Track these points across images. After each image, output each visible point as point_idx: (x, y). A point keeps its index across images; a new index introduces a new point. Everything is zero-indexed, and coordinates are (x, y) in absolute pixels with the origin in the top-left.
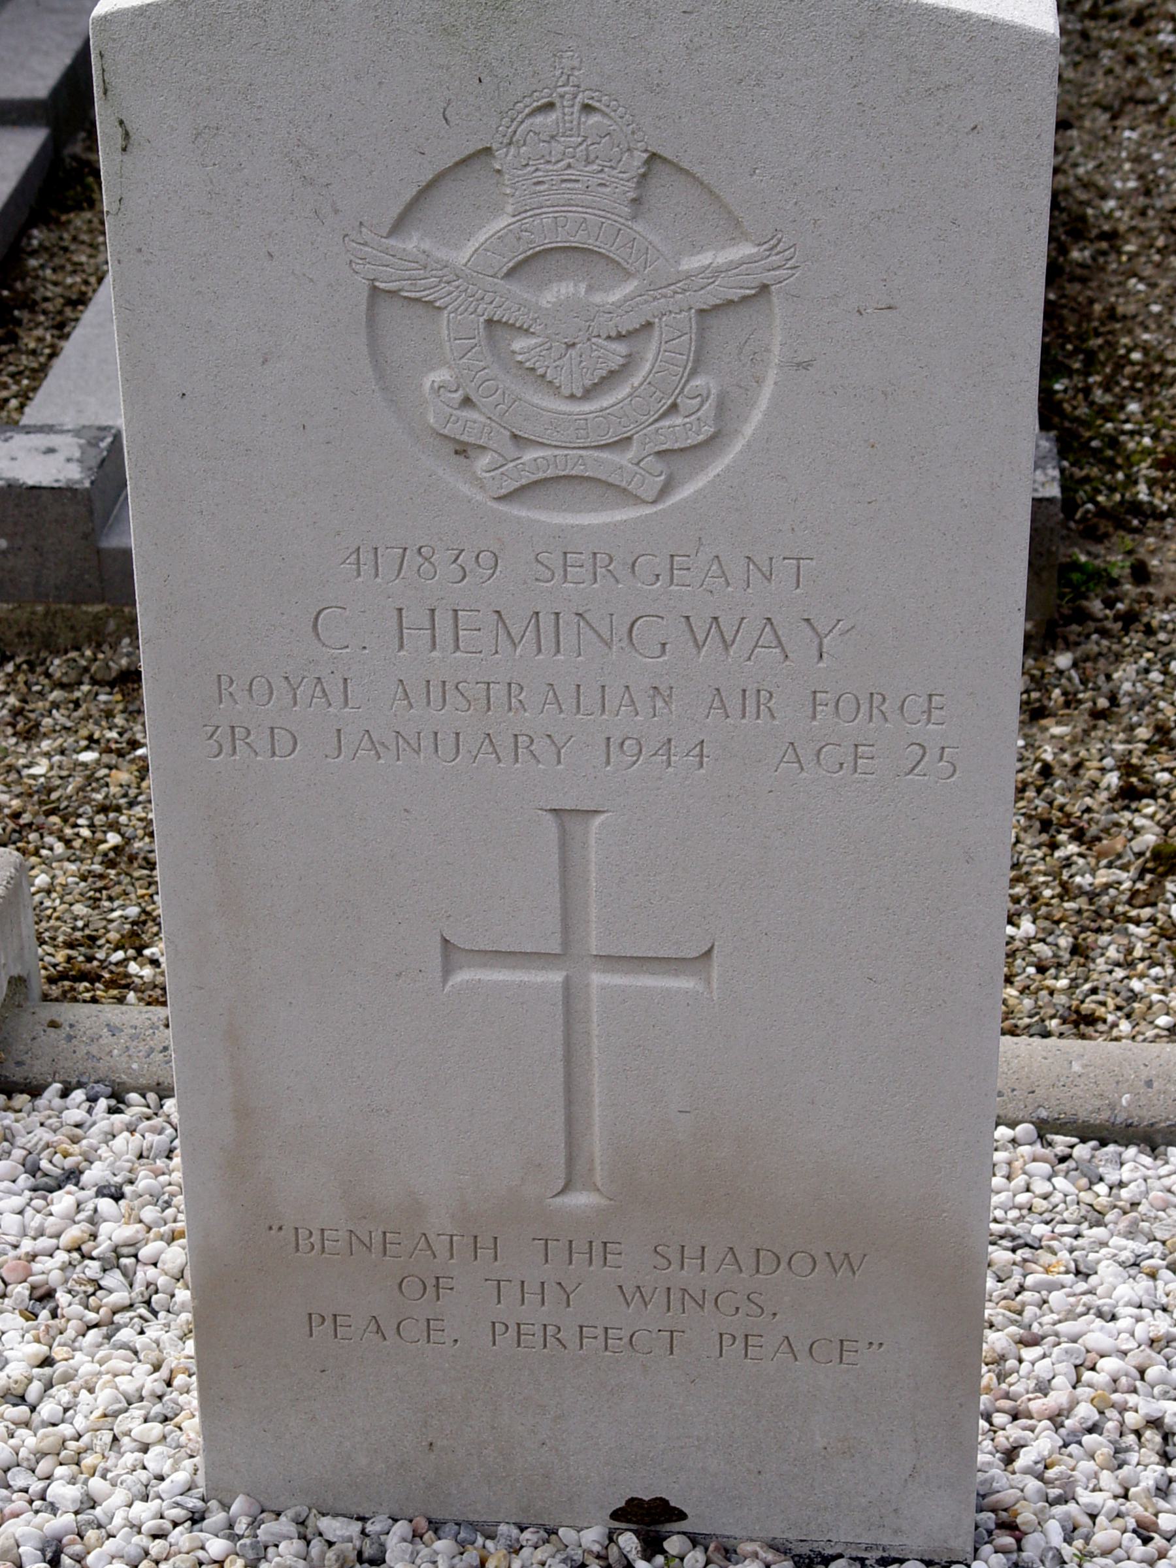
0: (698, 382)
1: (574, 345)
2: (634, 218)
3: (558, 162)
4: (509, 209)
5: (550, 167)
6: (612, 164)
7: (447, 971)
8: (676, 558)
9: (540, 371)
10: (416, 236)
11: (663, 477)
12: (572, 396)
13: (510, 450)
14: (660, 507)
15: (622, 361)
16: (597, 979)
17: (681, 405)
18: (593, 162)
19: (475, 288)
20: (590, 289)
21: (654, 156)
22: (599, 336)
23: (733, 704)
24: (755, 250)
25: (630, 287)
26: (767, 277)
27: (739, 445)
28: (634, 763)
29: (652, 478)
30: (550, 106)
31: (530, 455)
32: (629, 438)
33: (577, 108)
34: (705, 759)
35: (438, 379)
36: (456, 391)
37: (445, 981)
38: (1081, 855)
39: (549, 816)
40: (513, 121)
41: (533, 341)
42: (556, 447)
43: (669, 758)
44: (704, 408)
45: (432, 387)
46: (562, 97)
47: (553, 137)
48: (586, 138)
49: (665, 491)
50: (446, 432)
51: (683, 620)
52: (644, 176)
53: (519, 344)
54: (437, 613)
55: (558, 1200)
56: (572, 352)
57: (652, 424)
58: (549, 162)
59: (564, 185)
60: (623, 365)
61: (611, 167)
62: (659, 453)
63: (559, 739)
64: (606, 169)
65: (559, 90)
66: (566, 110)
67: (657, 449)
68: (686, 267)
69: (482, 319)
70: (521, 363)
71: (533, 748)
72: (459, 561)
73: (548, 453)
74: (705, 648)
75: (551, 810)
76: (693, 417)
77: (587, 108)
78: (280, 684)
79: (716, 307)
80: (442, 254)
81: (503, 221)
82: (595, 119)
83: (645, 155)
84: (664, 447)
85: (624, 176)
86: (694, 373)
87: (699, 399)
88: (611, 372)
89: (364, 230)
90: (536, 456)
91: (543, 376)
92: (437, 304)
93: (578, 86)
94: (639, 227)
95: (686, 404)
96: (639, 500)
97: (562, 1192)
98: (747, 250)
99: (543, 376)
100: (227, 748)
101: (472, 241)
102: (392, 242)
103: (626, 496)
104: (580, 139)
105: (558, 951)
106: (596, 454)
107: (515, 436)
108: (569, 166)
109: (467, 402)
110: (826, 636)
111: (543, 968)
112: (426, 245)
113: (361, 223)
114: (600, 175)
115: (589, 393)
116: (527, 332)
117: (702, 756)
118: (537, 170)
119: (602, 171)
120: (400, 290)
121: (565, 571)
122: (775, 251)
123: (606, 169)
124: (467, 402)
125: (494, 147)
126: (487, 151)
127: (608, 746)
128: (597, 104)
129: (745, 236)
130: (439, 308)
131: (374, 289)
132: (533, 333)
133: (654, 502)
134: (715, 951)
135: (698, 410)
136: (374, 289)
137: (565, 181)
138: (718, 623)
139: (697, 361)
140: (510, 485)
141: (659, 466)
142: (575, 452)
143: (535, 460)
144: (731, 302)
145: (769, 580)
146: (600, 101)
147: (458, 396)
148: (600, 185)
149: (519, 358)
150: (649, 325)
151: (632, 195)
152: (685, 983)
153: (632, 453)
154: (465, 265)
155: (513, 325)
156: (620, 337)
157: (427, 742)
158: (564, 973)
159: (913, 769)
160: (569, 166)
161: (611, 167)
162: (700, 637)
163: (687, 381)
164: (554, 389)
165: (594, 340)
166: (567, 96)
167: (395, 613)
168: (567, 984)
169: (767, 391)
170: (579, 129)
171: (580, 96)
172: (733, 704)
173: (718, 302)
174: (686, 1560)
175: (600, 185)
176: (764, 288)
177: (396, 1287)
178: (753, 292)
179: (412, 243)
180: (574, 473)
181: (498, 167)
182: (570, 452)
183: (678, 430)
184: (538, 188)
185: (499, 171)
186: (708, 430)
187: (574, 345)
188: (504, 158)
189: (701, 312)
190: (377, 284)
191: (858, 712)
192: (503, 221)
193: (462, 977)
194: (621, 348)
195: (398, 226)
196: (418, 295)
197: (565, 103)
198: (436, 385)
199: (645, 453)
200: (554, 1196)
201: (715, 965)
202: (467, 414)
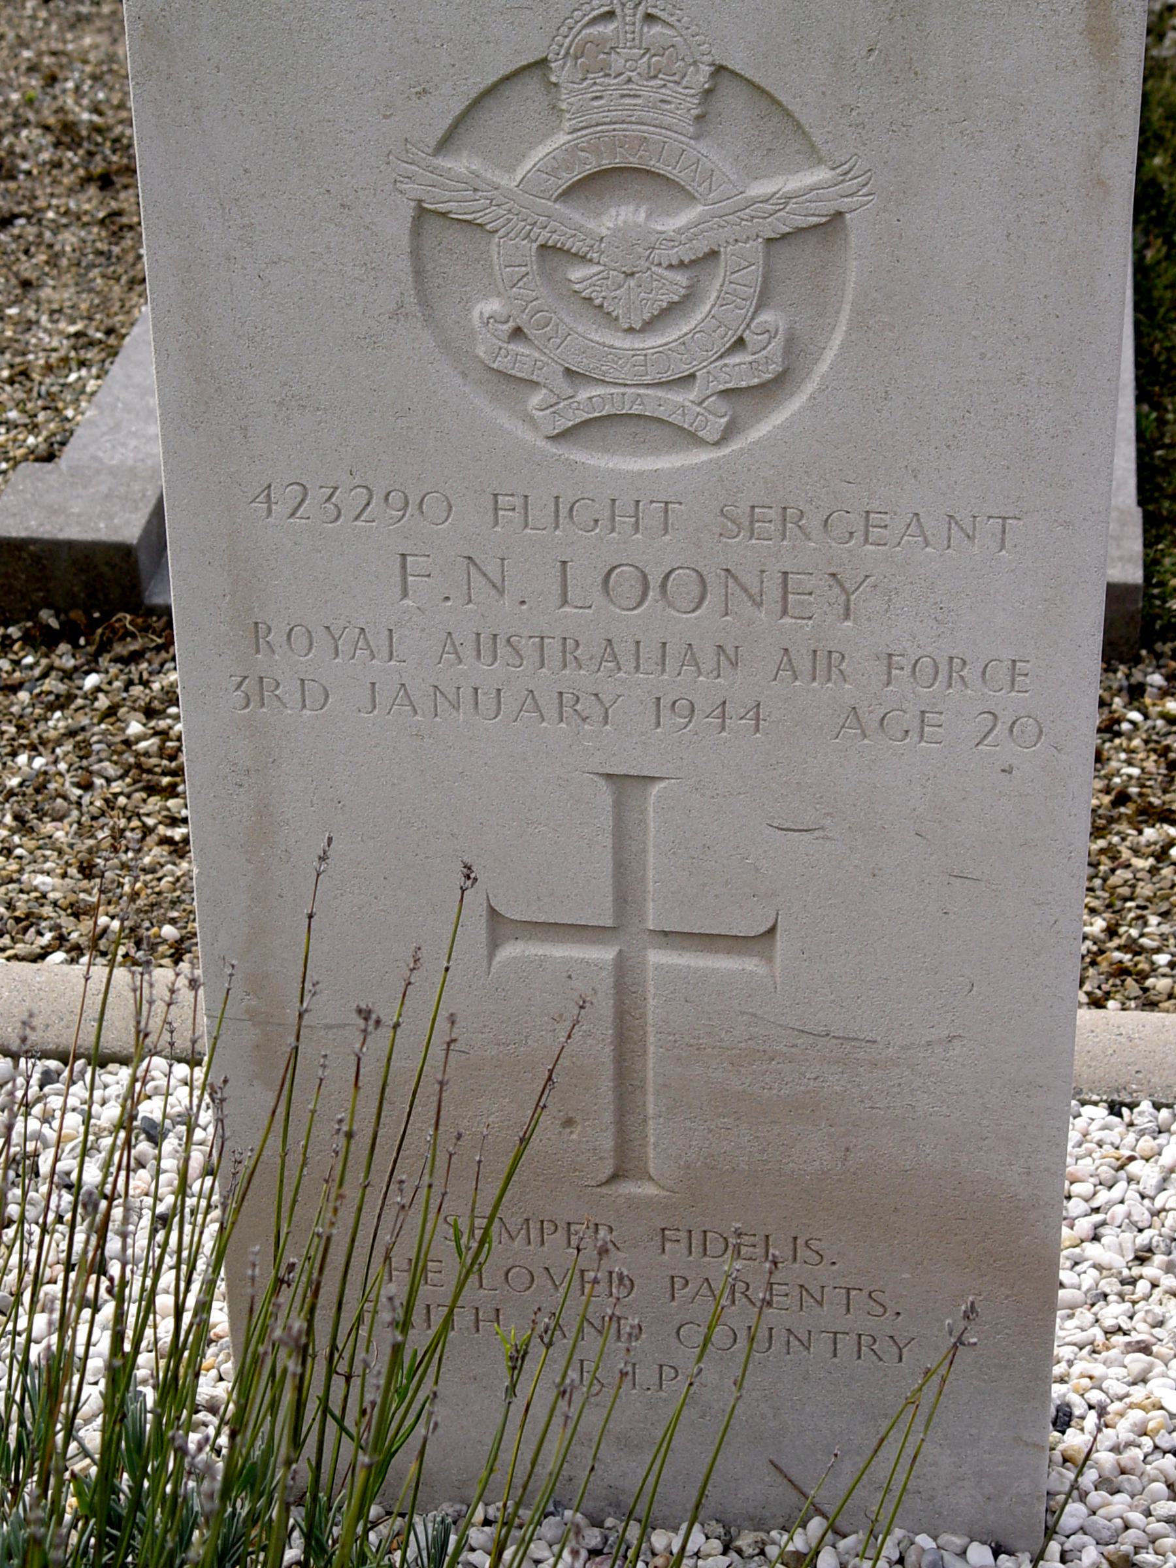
0: (766, 317)
1: (632, 274)
2: (696, 138)
4: (567, 125)
5: (606, 80)
6: (676, 78)
7: (494, 945)
8: (872, 515)
9: (597, 302)
12: (631, 330)
14: (726, 451)
15: (683, 292)
16: (657, 957)
17: (747, 339)
20: (649, 216)
21: (720, 70)
22: (660, 264)
26: (844, 204)
27: (810, 387)
37: (491, 956)
38: (32, 713)
39: (602, 782)
40: (571, 28)
41: (595, 269)
43: (724, 721)
44: (770, 347)
48: (648, 50)
50: (495, 366)
52: (708, 92)
53: (577, 273)
60: (684, 296)
61: (675, 82)
64: (670, 85)
66: (628, 18)
67: (722, 387)
69: (535, 245)
71: (578, 707)
72: (333, 500)
75: (608, 776)
77: (650, 18)
78: (320, 635)
79: (784, 236)
81: (562, 138)
82: (657, 29)
83: (713, 68)
84: (729, 386)
87: (766, 335)
91: (601, 306)
92: (488, 227)
94: (702, 147)
97: (614, 1178)
98: (821, 175)
99: (601, 306)
100: (255, 698)
102: (439, 161)
103: (692, 439)
104: (642, 52)
105: (609, 923)
106: (659, 393)
108: (629, 80)
110: (853, 593)
114: (663, 90)
115: (649, 326)
116: (583, 259)
117: (758, 719)
118: (595, 83)
119: (665, 85)
120: (450, 212)
125: (551, 56)
128: (659, 14)
132: (591, 260)
133: (717, 444)
139: (762, 294)
141: (723, 406)
142: (633, 390)
143: (590, 398)
148: (662, 101)
149: (577, 287)
150: (713, 254)
151: (695, 112)
152: (750, 964)
153: (693, 394)
155: (568, 251)
158: (617, 948)
160: (629, 80)
161: (675, 82)
163: (752, 319)
164: (611, 320)
167: (399, 559)
168: (620, 964)
170: (641, 42)
173: (788, 230)
175: (662, 101)
177: (674, 1334)
178: (824, 220)
179: (460, 164)
182: (627, 390)
183: (740, 370)
184: (595, 103)
185: (556, 85)
186: (774, 368)
187: (632, 274)
189: (769, 241)
190: (426, 205)
191: (935, 679)
192: (562, 138)
193: (510, 951)
194: (681, 278)
195: (445, 143)
197: (628, 12)
199: (709, 392)
200: (598, 1186)
201: (779, 944)
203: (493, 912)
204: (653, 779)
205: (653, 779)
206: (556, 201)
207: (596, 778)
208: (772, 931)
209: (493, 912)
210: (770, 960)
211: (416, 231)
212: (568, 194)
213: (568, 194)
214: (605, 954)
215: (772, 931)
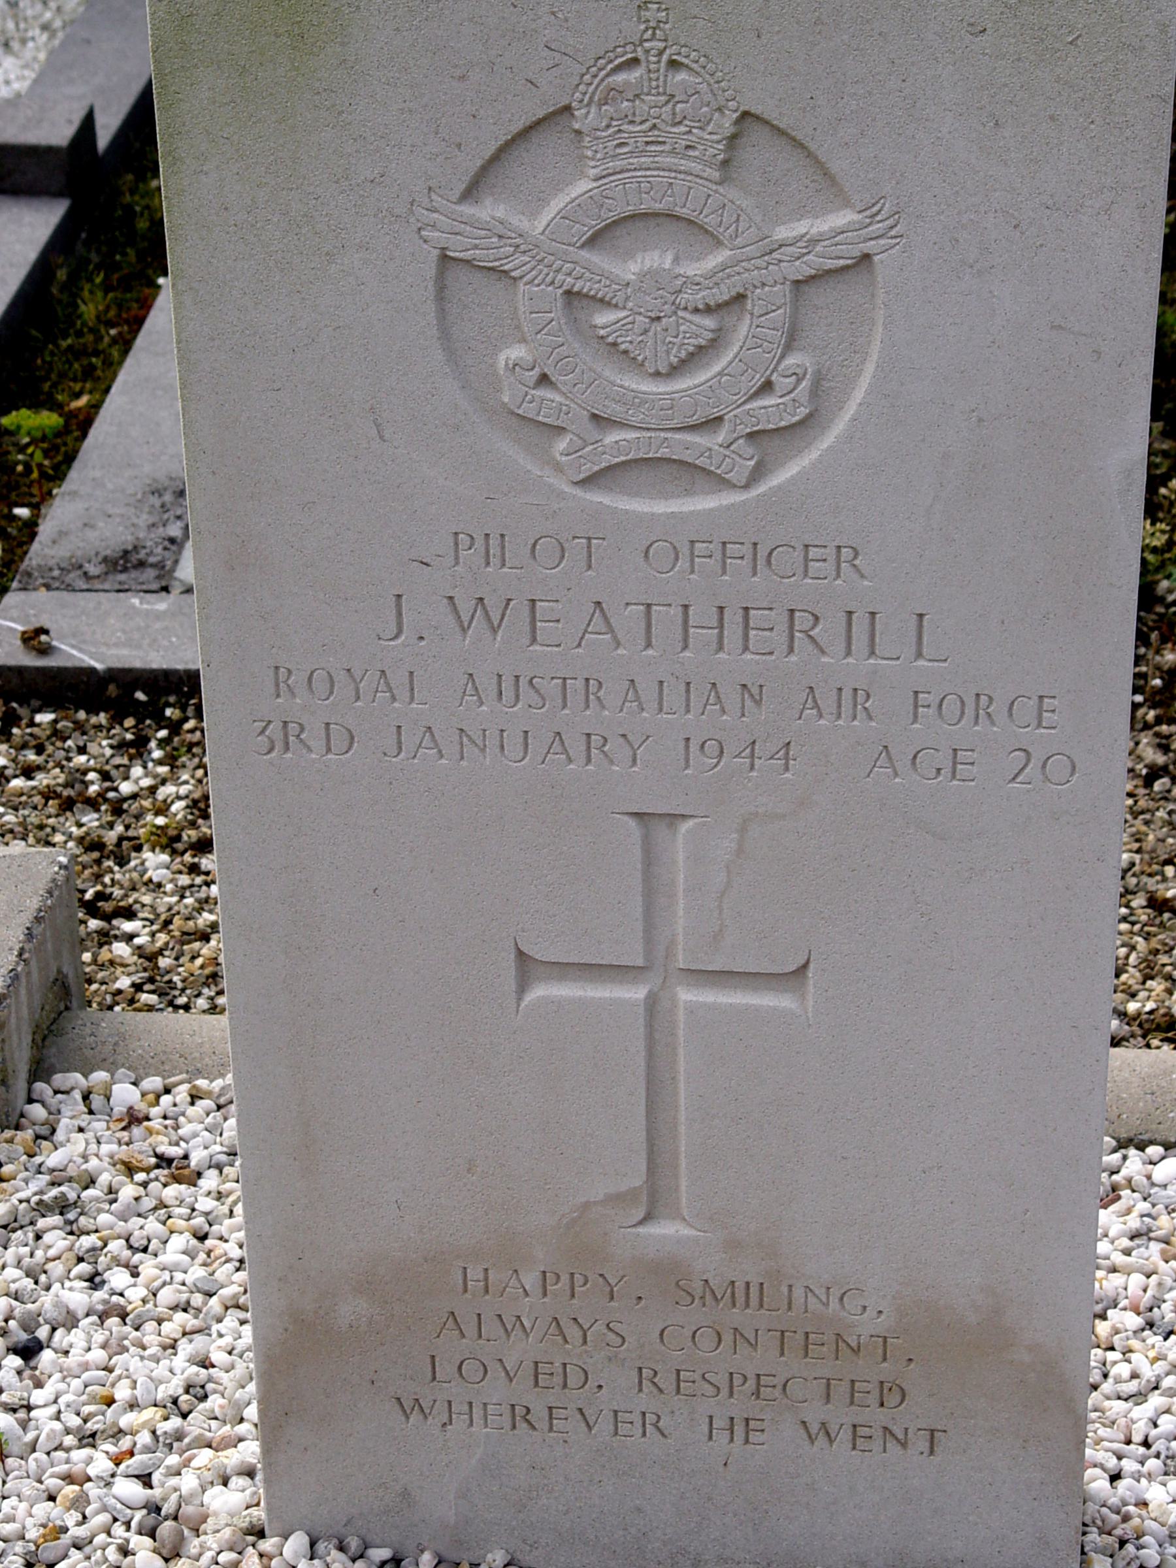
0: (790, 361)
1: (659, 318)
3: (642, 123)
5: (631, 128)
7: (522, 988)
10: (488, 201)
11: (752, 463)
12: (657, 374)
13: (592, 432)
15: (710, 335)
16: (686, 995)
18: (680, 123)
19: (553, 258)
20: (676, 260)
23: (828, 703)
24: (857, 217)
25: (720, 257)
27: (839, 426)
28: (716, 766)
29: (742, 461)
30: (635, 61)
31: (613, 437)
32: (720, 419)
33: (663, 64)
34: (792, 762)
35: (513, 357)
36: (532, 369)
37: (520, 1000)
39: (632, 823)
40: (595, 76)
42: (648, 429)
45: (507, 365)
46: (647, 51)
47: (637, 96)
49: (758, 473)
50: (520, 412)
51: (445, 601)
53: (603, 318)
54: (854, 616)
55: (641, 1230)
56: (657, 327)
57: (738, 407)
58: (632, 122)
59: (648, 148)
62: (751, 436)
63: (635, 739)
64: (694, 131)
65: (646, 45)
68: (780, 237)
69: (561, 291)
70: (602, 337)
73: (632, 435)
74: (470, 632)
76: (787, 398)
77: (673, 64)
80: (520, 222)
81: (583, 186)
82: (682, 76)
85: (715, 137)
86: (788, 348)
88: (700, 347)
89: (434, 197)
90: (618, 438)
93: (665, 40)
95: (782, 383)
96: (723, 483)
98: (843, 218)
100: (279, 746)
101: (546, 209)
107: (595, 417)
108: (654, 126)
109: (544, 379)
111: (621, 982)
112: (500, 213)
113: (430, 189)
115: (675, 370)
118: (620, 131)
119: (690, 132)
121: (692, 561)
122: (879, 218)
123: (694, 131)
124: (544, 379)
126: (567, 109)
127: (687, 747)
128: (685, 61)
129: (847, 204)
130: (515, 279)
131: (445, 258)
133: (746, 487)
134: (812, 966)
135: (794, 389)
136: (445, 258)
137: (652, 142)
138: (483, 604)
140: (588, 469)
144: (829, 272)
145: (494, 630)
146: (687, 57)
147: (536, 373)
149: (602, 332)
152: (784, 1001)
153: (721, 436)
154: (543, 233)
156: (708, 310)
157: (492, 742)
159: (1016, 776)
162: (465, 618)
165: (680, 313)
166: (652, 52)
167: (786, 614)
168: (652, 1002)
169: (870, 368)
171: (668, 52)
172: (828, 703)
174: (159, 1296)
176: (867, 257)
179: (489, 210)
180: (658, 455)
181: (577, 126)
186: (802, 412)
187: (659, 318)
188: (586, 118)
189: (797, 282)
190: (449, 253)
192: (583, 186)
193: (539, 992)
194: (709, 322)
195: (470, 193)
196: (491, 264)
198: (511, 362)
202: (544, 393)
203: (520, 954)
204: (684, 817)
205: (684, 817)
206: (582, 246)
207: (626, 818)
208: (805, 966)
209: (520, 954)
210: (803, 997)
211: (441, 289)
212: (593, 241)
213: (593, 241)
214: (638, 993)
215: (805, 966)
